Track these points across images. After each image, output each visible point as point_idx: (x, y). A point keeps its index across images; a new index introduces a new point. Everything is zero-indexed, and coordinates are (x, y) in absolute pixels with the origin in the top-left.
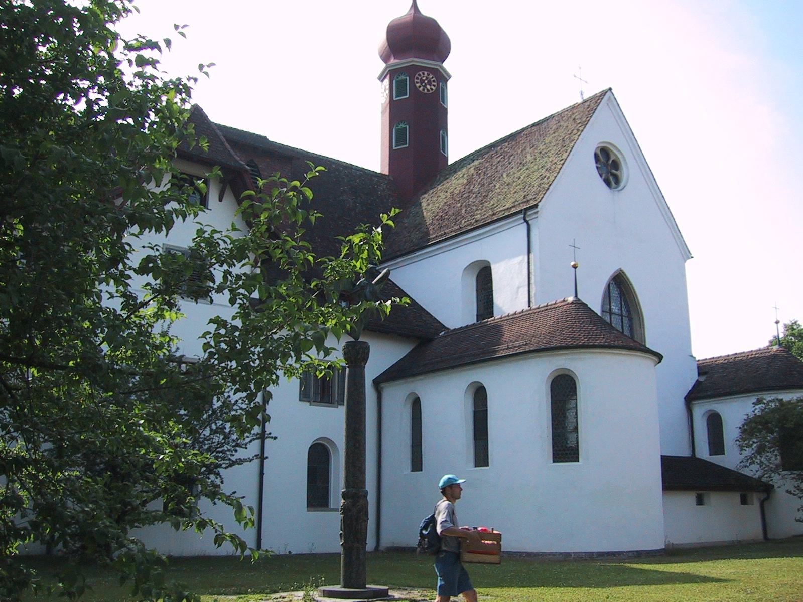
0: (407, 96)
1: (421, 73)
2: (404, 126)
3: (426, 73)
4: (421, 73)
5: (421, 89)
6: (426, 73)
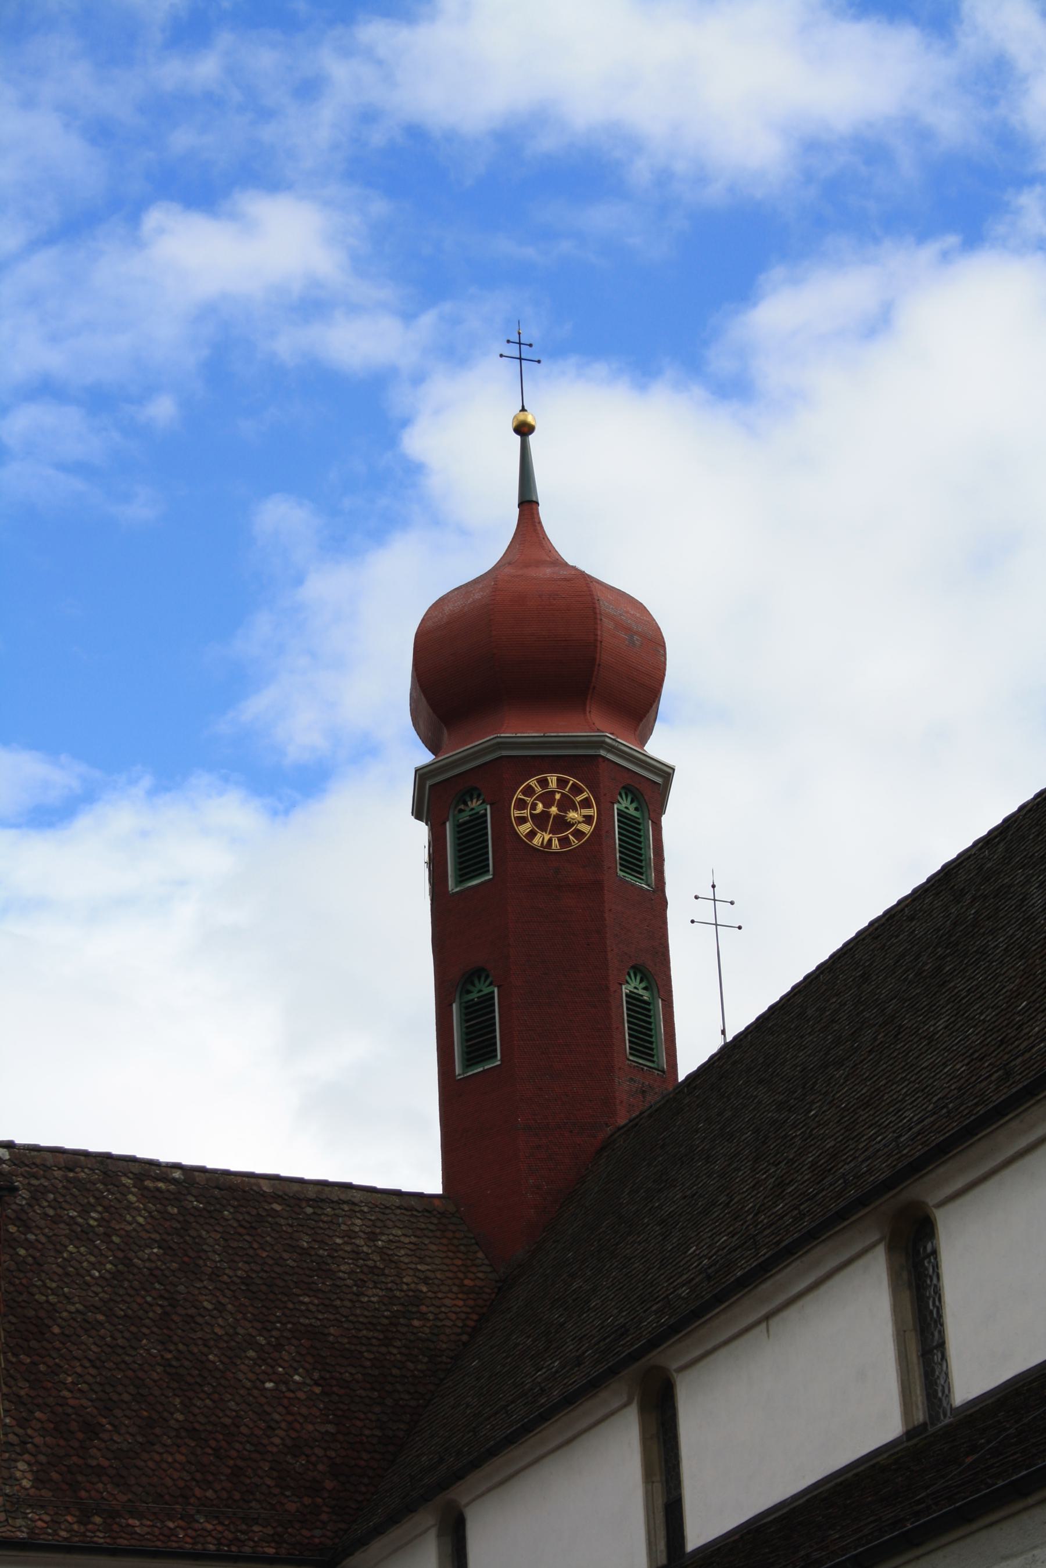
1: (533, 782)
2: (486, 991)
3: (553, 780)
6: (553, 780)
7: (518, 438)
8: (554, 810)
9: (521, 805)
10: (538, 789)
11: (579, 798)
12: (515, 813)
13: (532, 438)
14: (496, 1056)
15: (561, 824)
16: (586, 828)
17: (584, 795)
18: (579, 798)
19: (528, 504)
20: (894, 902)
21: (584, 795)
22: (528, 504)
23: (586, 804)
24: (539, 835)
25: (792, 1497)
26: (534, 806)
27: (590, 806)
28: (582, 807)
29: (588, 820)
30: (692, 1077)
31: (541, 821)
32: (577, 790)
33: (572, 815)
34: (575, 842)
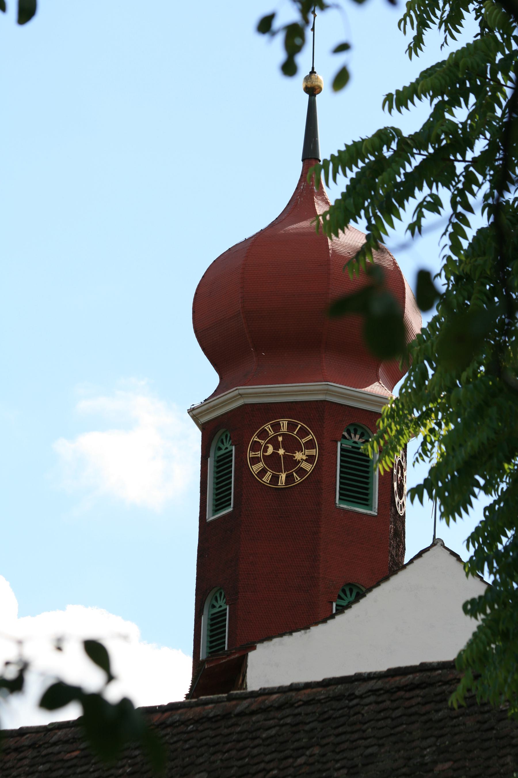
0: (230, 509)
1: (268, 427)
3: (284, 424)
4: (268, 427)
5: (267, 478)
6: (284, 424)
7: (307, 96)
8: (281, 452)
9: (256, 447)
10: (271, 433)
11: (304, 441)
12: (250, 454)
13: (318, 98)
14: (230, 504)
15: (291, 463)
16: (308, 467)
17: (310, 437)
18: (304, 441)
19: (313, 68)
20: (200, 472)
21: (310, 437)
22: (313, 68)
23: (310, 445)
24: (269, 473)
25: (370, 674)
26: (266, 449)
27: (314, 447)
28: (307, 448)
29: (310, 459)
30: (414, 189)
31: (273, 461)
32: (303, 433)
33: (299, 456)
34: (298, 479)
